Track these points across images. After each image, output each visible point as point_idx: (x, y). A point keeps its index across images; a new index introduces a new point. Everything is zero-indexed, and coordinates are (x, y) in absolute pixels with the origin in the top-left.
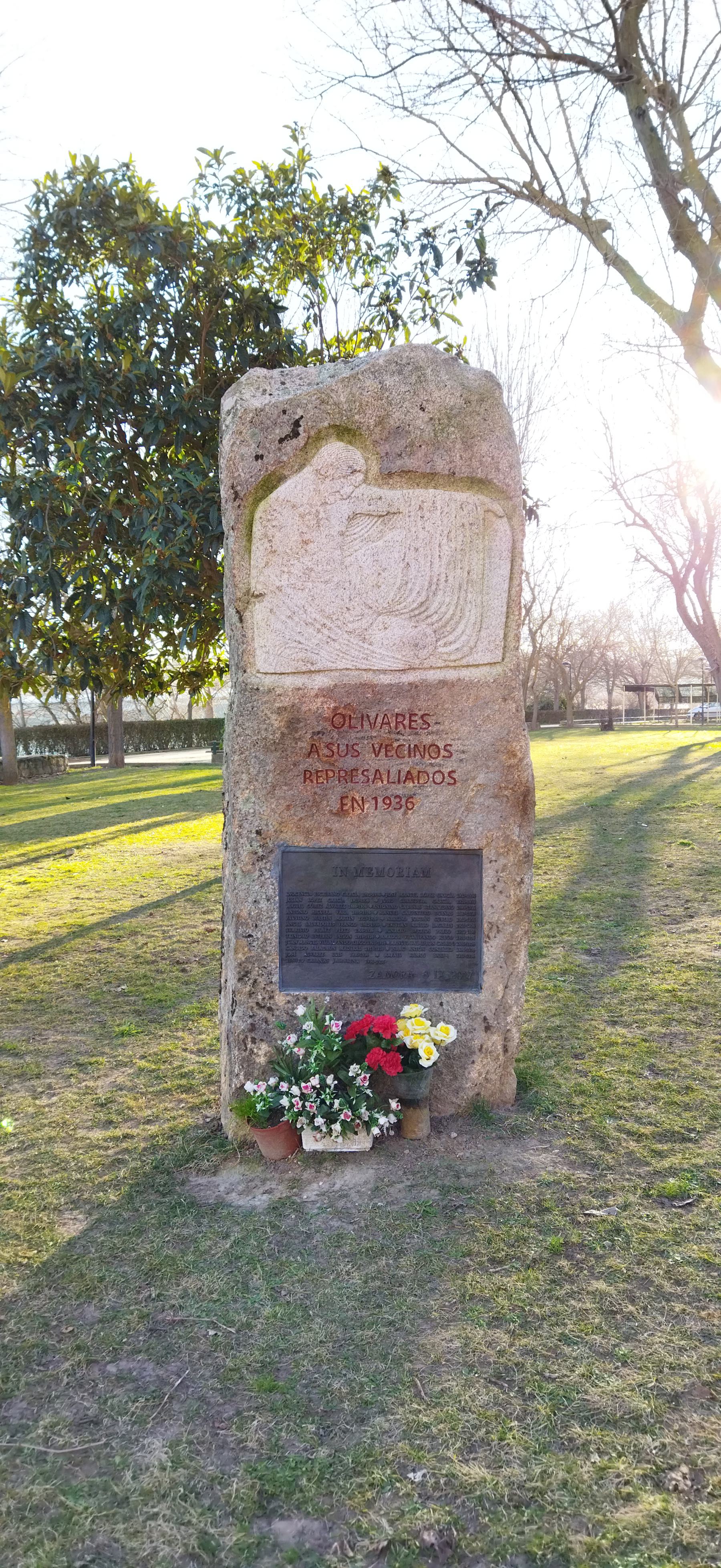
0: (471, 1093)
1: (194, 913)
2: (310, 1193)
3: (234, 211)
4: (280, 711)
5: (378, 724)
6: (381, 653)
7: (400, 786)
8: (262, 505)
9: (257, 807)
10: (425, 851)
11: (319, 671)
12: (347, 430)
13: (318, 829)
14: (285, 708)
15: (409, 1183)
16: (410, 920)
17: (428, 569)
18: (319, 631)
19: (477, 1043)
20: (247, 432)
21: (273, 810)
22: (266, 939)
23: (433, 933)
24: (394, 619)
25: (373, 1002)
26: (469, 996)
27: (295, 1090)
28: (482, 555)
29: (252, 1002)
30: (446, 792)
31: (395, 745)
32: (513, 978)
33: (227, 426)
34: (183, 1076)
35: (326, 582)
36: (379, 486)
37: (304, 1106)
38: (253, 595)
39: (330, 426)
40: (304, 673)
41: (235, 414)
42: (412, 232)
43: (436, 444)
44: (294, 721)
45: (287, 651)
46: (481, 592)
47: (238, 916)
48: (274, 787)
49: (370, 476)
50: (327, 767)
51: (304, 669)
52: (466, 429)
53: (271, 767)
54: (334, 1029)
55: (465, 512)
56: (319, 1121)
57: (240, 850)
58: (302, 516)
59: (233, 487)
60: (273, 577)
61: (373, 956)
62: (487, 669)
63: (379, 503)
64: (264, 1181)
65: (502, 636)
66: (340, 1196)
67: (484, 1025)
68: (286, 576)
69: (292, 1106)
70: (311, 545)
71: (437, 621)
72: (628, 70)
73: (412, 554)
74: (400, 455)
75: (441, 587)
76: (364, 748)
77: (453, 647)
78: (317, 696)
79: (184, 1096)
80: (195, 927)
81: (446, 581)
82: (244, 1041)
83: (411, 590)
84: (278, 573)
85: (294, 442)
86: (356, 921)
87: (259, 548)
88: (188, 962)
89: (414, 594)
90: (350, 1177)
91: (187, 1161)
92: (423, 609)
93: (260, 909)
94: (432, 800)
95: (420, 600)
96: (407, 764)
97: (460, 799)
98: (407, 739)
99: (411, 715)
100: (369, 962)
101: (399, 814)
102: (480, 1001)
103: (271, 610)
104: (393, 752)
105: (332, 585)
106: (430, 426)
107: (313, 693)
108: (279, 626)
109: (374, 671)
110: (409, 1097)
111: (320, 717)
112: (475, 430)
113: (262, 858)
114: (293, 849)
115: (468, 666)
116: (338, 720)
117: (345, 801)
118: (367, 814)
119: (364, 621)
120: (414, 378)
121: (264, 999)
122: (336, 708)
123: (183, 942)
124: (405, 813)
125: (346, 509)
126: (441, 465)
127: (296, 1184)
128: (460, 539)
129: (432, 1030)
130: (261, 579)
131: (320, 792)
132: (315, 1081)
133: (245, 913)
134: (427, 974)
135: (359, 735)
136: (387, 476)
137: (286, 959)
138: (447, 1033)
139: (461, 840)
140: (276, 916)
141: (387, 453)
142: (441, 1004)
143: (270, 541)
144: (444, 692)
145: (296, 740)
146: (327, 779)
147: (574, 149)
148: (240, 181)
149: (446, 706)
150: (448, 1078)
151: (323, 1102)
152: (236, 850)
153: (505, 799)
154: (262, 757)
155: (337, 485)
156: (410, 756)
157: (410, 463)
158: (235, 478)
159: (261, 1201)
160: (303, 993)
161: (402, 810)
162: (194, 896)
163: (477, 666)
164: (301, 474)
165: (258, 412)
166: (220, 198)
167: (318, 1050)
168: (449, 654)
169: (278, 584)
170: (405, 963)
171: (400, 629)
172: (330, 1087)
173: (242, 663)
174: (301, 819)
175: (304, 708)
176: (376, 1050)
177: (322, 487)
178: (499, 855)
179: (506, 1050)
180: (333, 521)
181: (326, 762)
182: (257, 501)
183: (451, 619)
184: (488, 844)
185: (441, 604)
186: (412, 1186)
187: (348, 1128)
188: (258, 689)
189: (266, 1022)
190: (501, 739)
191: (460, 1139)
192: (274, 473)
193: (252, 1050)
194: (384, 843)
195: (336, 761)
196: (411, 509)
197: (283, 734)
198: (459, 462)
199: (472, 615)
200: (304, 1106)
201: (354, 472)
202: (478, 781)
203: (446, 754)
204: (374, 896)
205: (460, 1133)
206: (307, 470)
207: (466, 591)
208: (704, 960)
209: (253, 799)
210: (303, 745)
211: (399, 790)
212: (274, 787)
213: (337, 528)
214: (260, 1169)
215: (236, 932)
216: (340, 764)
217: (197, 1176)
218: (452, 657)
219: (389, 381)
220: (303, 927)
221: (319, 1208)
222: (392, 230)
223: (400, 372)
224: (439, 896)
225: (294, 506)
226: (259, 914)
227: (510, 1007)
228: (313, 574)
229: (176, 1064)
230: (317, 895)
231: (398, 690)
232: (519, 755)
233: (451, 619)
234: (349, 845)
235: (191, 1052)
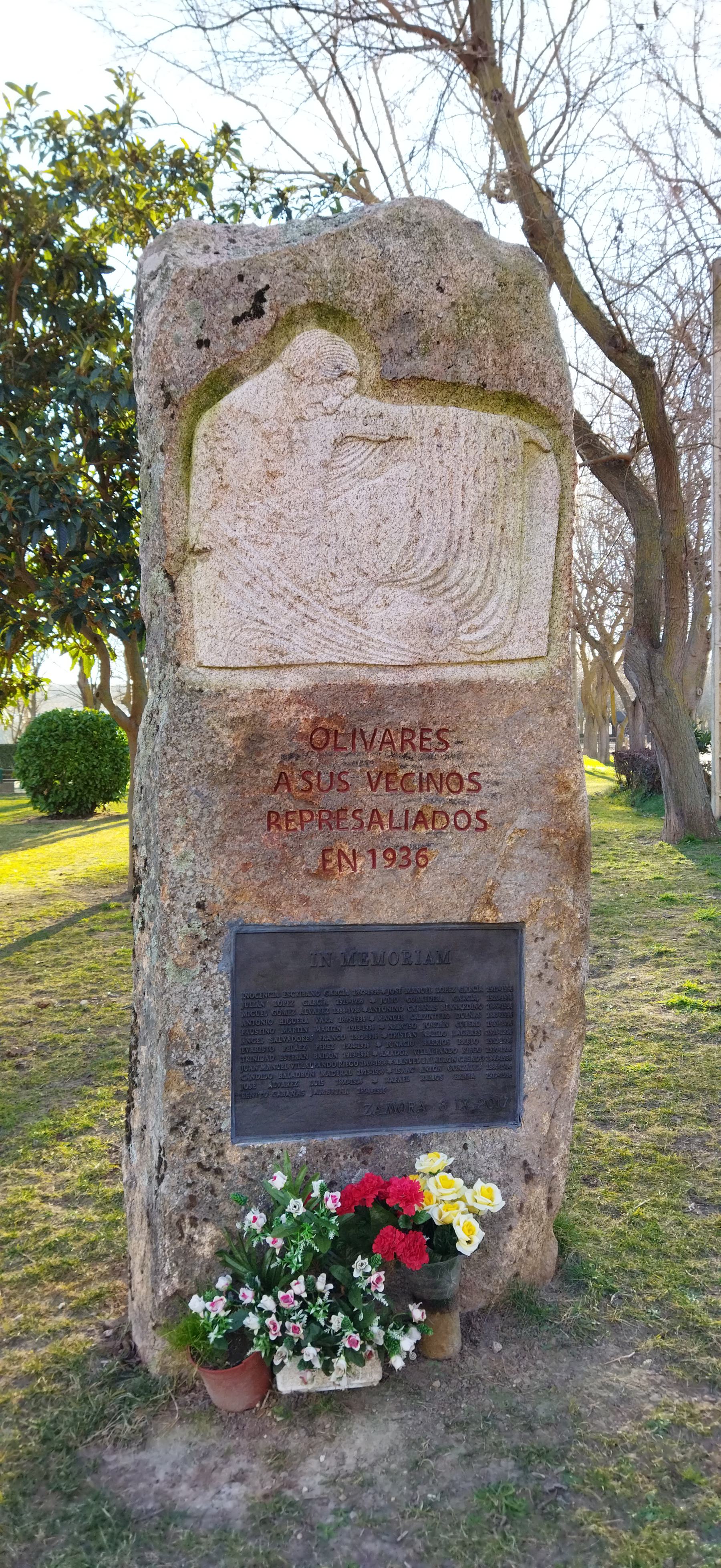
0: (508, 1275)
1: (17, 981)
2: (311, 1479)
3: (48, 159)
4: (234, 724)
5: (377, 744)
6: (379, 639)
7: (407, 833)
8: (207, 417)
9: (198, 868)
10: (443, 928)
11: (290, 666)
12: (333, 312)
13: (289, 898)
14: (243, 720)
15: (463, 1451)
16: (421, 1027)
17: (446, 521)
18: (291, 606)
20: (184, 303)
21: (222, 871)
22: (212, 1067)
23: (454, 1045)
24: (399, 592)
25: (367, 1150)
26: (504, 1133)
27: (267, 1303)
28: (520, 505)
29: (191, 1163)
30: (472, 843)
31: (401, 773)
33: (151, 296)
34: (51, 1248)
35: (302, 535)
36: (378, 398)
37: (283, 1329)
38: (192, 551)
40: (268, 668)
41: (165, 277)
42: (265, 191)
43: (459, 342)
44: (255, 737)
45: (245, 634)
46: (519, 557)
47: (170, 1034)
48: (223, 837)
49: (365, 383)
50: (302, 806)
51: (270, 661)
52: (501, 323)
53: (220, 807)
54: (330, 1205)
55: (499, 442)
56: (310, 1352)
57: (173, 933)
58: (267, 436)
59: (163, 386)
60: (223, 524)
61: (368, 1083)
62: (525, 666)
63: (379, 422)
64: (226, 1455)
65: (546, 620)
66: (362, 1485)
67: (523, 1173)
68: (242, 524)
69: (264, 1329)
70: (280, 480)
71: (459, 597)
72: (477, 56)
74: (409, 354)
75: (464, 547)
76: (356, 777)
77: (480, 634)
78: (289, 701)
79: (61, 1286)
80: (22, 1001)
81: (472, 539)
82: (179, 1223)
83: (423, 550)
84: (231, 518)
85: (256, 323)
86: (344, 1032)
87: (202, 480)
88: (23, 1053)
89: (427, 557)
90: (368, 1442)
91: (96, 1426)
92: (439, 578)
93: (204, 1022)
94: (453, 852)
95: (436, 565)
96: (417, 802)
97: (494, 850)
98: (418, 765)
99: (423, 730)
100: (363, 1093)
101: (406, 874)
102: (518, 1140)
103: (221, 574)
104: (397, 784)
106: (451, 315)
107: (283, 697)
108: (232, 597)
109: (369, 666)
110: (434, 1297)
111: (293, 733)
112: (513, 325)
113: (205, 944)
114: (251, 929)
115: (499, 662)
116: (319, 737)
117: (329, 856)
118: (361, 874)
119: (357, 593)
120: (426, 245)
121: (209, 1156)
122: (316, 720)
123: (11, 1024)
124: (415, 872)
125: (331, 428)
126: (467, 373)
127: (280, 1460)
128: (491, 480)
129: (468, 1194)
130: (206, 526)
131: (291, 843)
132: (299, 1287)
133: (180, 1029)
134: (446, 1105)
135: (348, 759)
136: (390, 384)
138: (489, 1197)
139: (496, 910)
140: (227, 1030)
141: (391, 350)
142: (465, 1147)
143: (219, 470)
145: (258, 767)
146: (302, 823)
147: (400, 157)
148: (55, 126)
149: (471, 718)
151: (311, 1319)
152: (166, 932)
153: (554, 850)
154: (206, 793)
155: (318, 392)
156: (421, 790)
157: (424, 366)
158: (164, 372)
159: (231, 1499)
160: (267, 1144)
161: (412, 867)
162: (12, 959)
163: (512, 661)
164: (265, 373)
165: (202, 274)
166: (32, 141)
167: (307, 1238)
168: (474, 643)
169: (231, 534)
170: (414, 1089)
171: (405, 606)
172: (322, 1295)
173: (174, 652)
174: (264, 883)
175: (271, 720)
176: (388, 1229)
177: (296, 395)
178: (547, 929)
179: (549, 1205)
180: (313, 446)
181: (300, 799)
182: (200, 410)
183: (479, 593)
184: (533, 915)
185: (465, 572)
186: (469, 1455)
187: (356, 1358)
188: (201, 691)
189: (213, 1192)
190: (549, 766)
191: (506, 1353)
192: (225, 368)
193: (191, 1238)
194: (385, 915)
195: (316, 797)
196: (424, 433)
197: (238, 758)
198: (492, 370)
199: (506, 589)
200: (283, 1329)
203: (473, 786)
204: (370, 994)
205: (505, 1342)
206: (274, 370)
207: (499, 554)
208: (660, 1025)
209: (192, 856)
210: (267, 773)
211: (407, 839)
212: (223, 837)
213: (319, 456)
214: (214, 1431)
215: (168, 1057)
216: (321, 802)
217: (114, 1451)
218: (479, 649)
219: (394, 245)
220: (267, 1045)
221: (335, 1512)
222: (240, 189)
223: (408, 235)
224: (462, 991)
225: (255, 421)
226: (201, 1030)
227: (558, 1144)
228: (283, 522)
229: (38, 1226)
230: (287, 995)
231: (406, 695)
232: (574, 787)
233: (479, 593)
234: (335, 921)
235: (56, 1203)
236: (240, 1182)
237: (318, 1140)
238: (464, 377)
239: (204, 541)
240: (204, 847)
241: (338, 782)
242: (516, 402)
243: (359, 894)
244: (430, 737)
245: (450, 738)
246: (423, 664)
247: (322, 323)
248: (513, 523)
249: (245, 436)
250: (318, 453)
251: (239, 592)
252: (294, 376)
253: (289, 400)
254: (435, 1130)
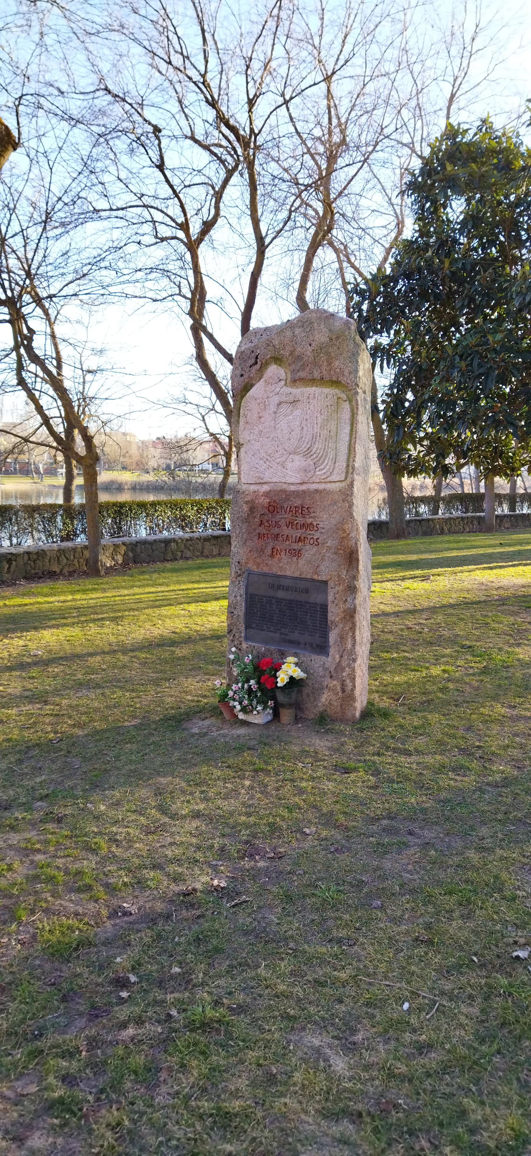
4: (247, 502)
8: (244, 399)
19: (326, 683)
26: (323, 658)
32: (345, 652)
35: (268, 438)
39: (271, 358)
53: (244, 531)
58: (259, 404)
61: (283, 630)
62: (339, 484)
73: (304, 422)
76: (282, 523)
94: (309, 552)
95: (308, 446)
96: (299, 533)
98: (300, 520)
100: (281, 634)
101: (295, 558)
105: (270, 439)
113: (240, 575)
116: (271, 508)
122: (270, 502)
125: (276, 400)
126: (316, 374)
136: (295, 382)
137: (248, 626)
144: (317, 496)
150: (312, 699)
168: (321, 475)
170: (295, 636)
171: (298, 462)
178: (336, 585)
182: (243, 397)
192: (248, 382)
194: (288, 573)
199: (331, 455)
201: (280, 380)
202: (328, 544)
213: (273, 410)
223: (303, 326)
227: (344, 668)
231: (297, 494)
237: (268, 647)
238: (315, 377)
241: (277, 524)
242: (335, 383)
243: (281, 565)
244: (303, 510)
248: (333, 428)
250: (273, 408)
252: (267, 383)
253: (266, 391)
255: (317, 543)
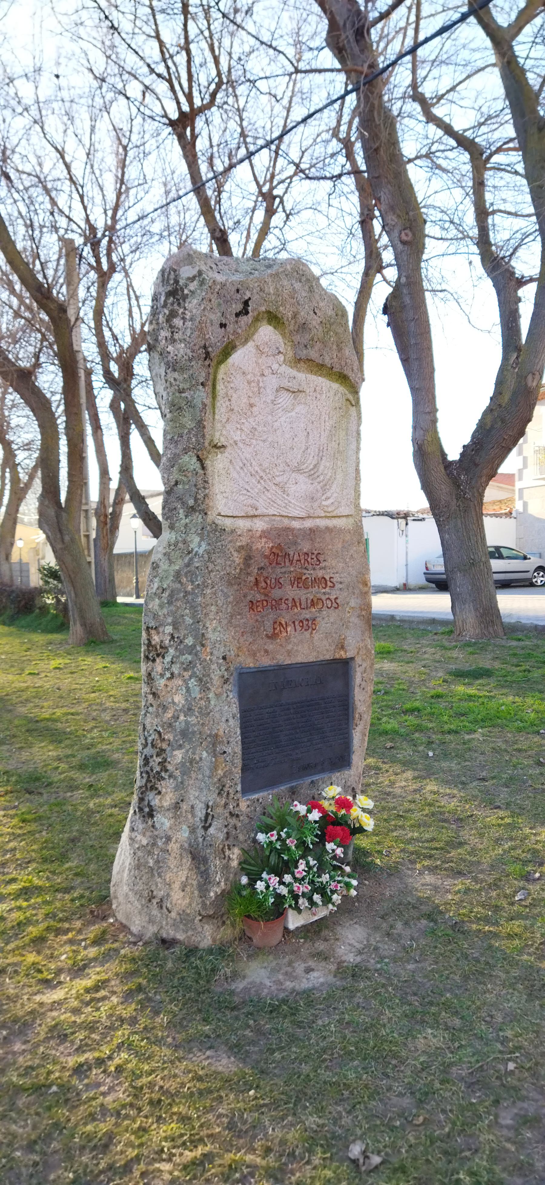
30: (333, 615)
35: (264, 441)
50: (263, 598)
53: (231, 599)
58: (249, 383)
62: (344, 519)
68: (239, 432)
78: (261, 537)
85: (245, 318)
87: (222, 405)
94: (327, 621)
95: (314, 463)
101: (307, 634)
107: (258, 535)
108: (235, 475)
135: (283, 570)
136: (297, 361)
157: (313, 354)
158: (206, 340)
163: (339, 517)
171: (300, 486)
177: (260, 361)
180: (268, 391)
182: (221, 362)
206: (250, 344)
236: (247, 820)
237: (275, 791)
239: (223, 441)
240: (225, 622)
241: (279, 584)
243: (289, 647)
244: (316, 558)
245: (321, 558)
246: (309, 517)
247: (269, 323)
249: (239, 381)
251: (238, 473)
254: (322, 776)
255: (336, 605)
